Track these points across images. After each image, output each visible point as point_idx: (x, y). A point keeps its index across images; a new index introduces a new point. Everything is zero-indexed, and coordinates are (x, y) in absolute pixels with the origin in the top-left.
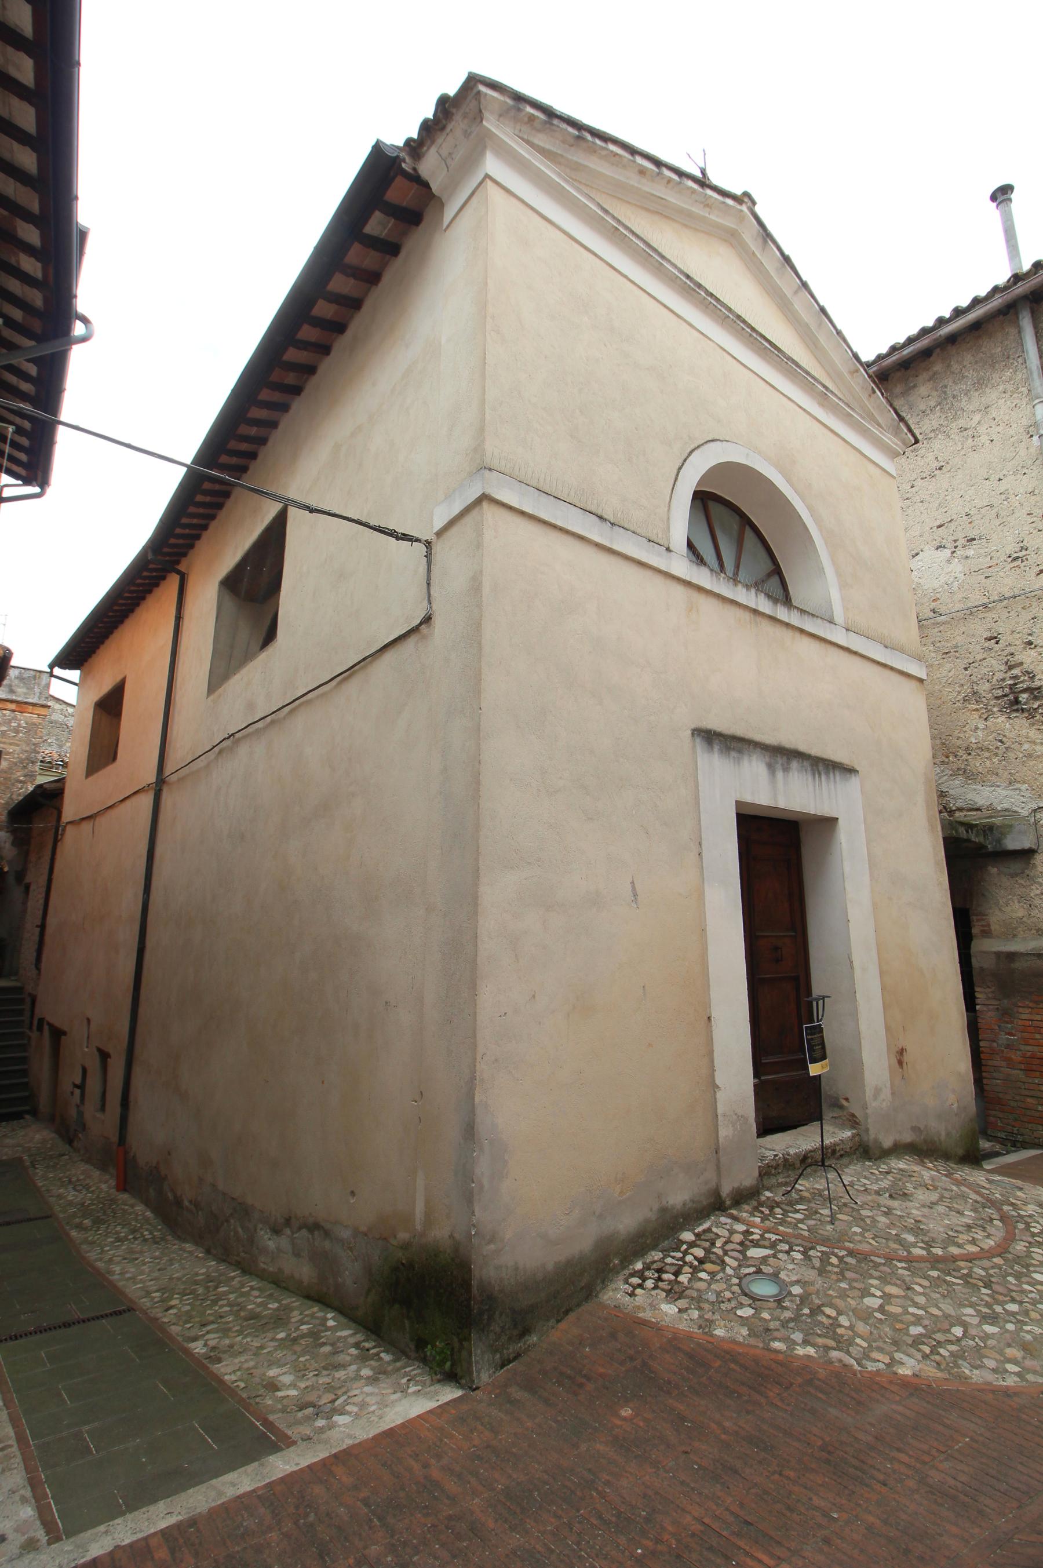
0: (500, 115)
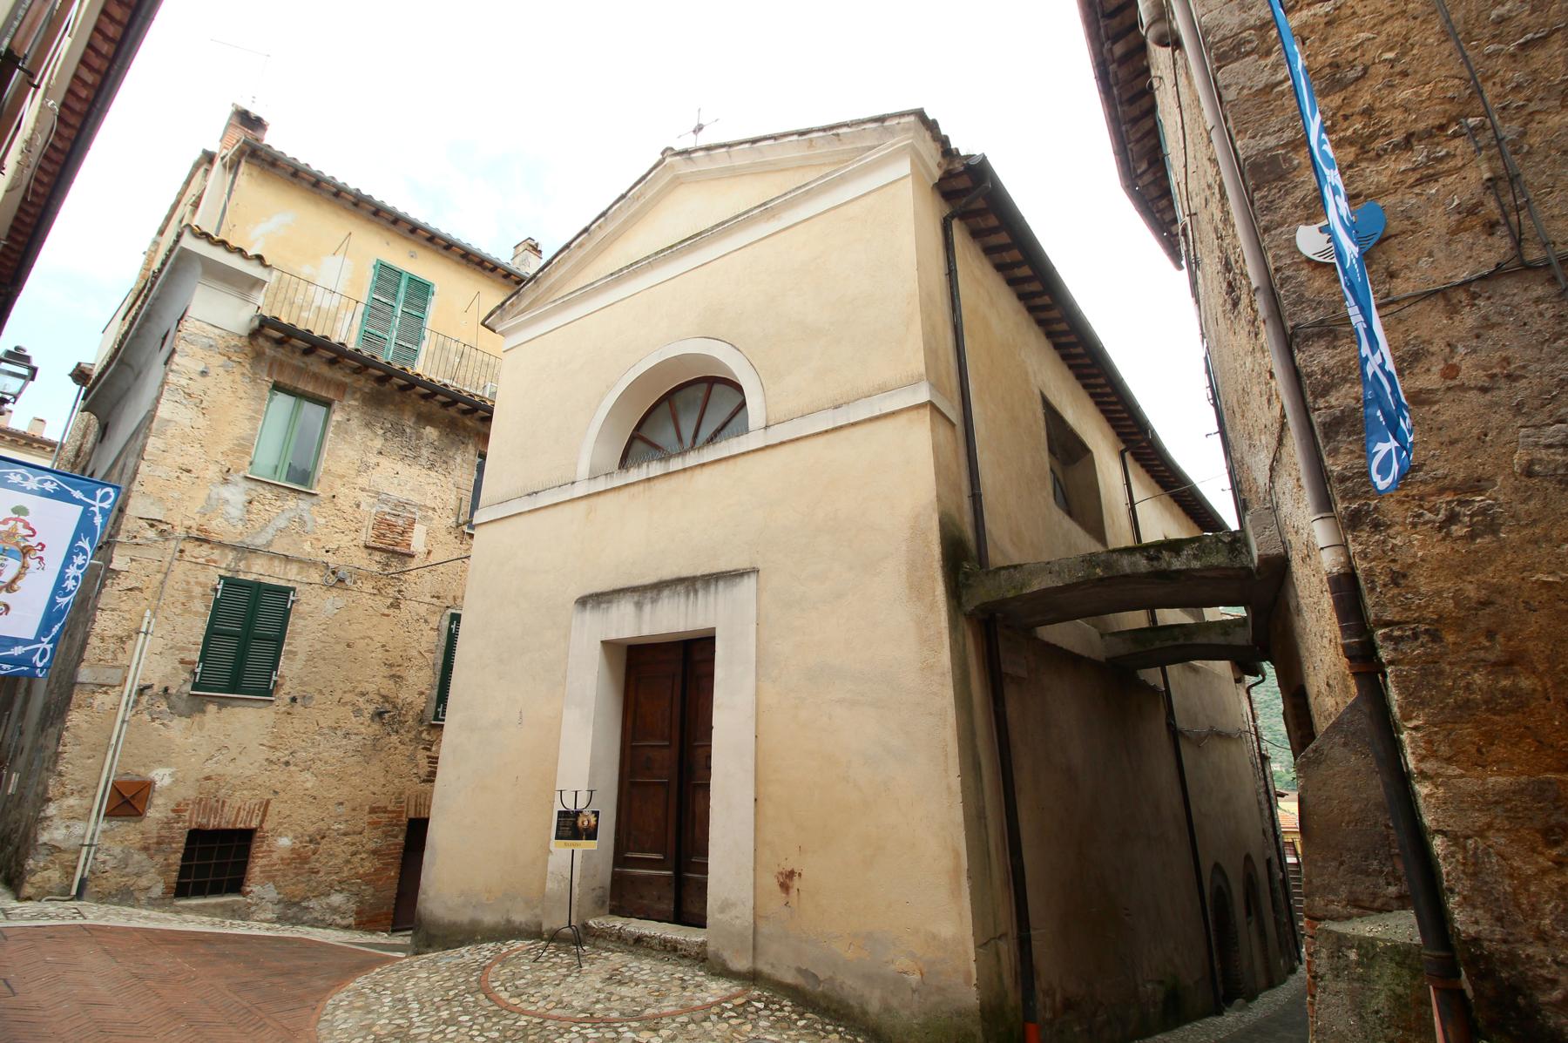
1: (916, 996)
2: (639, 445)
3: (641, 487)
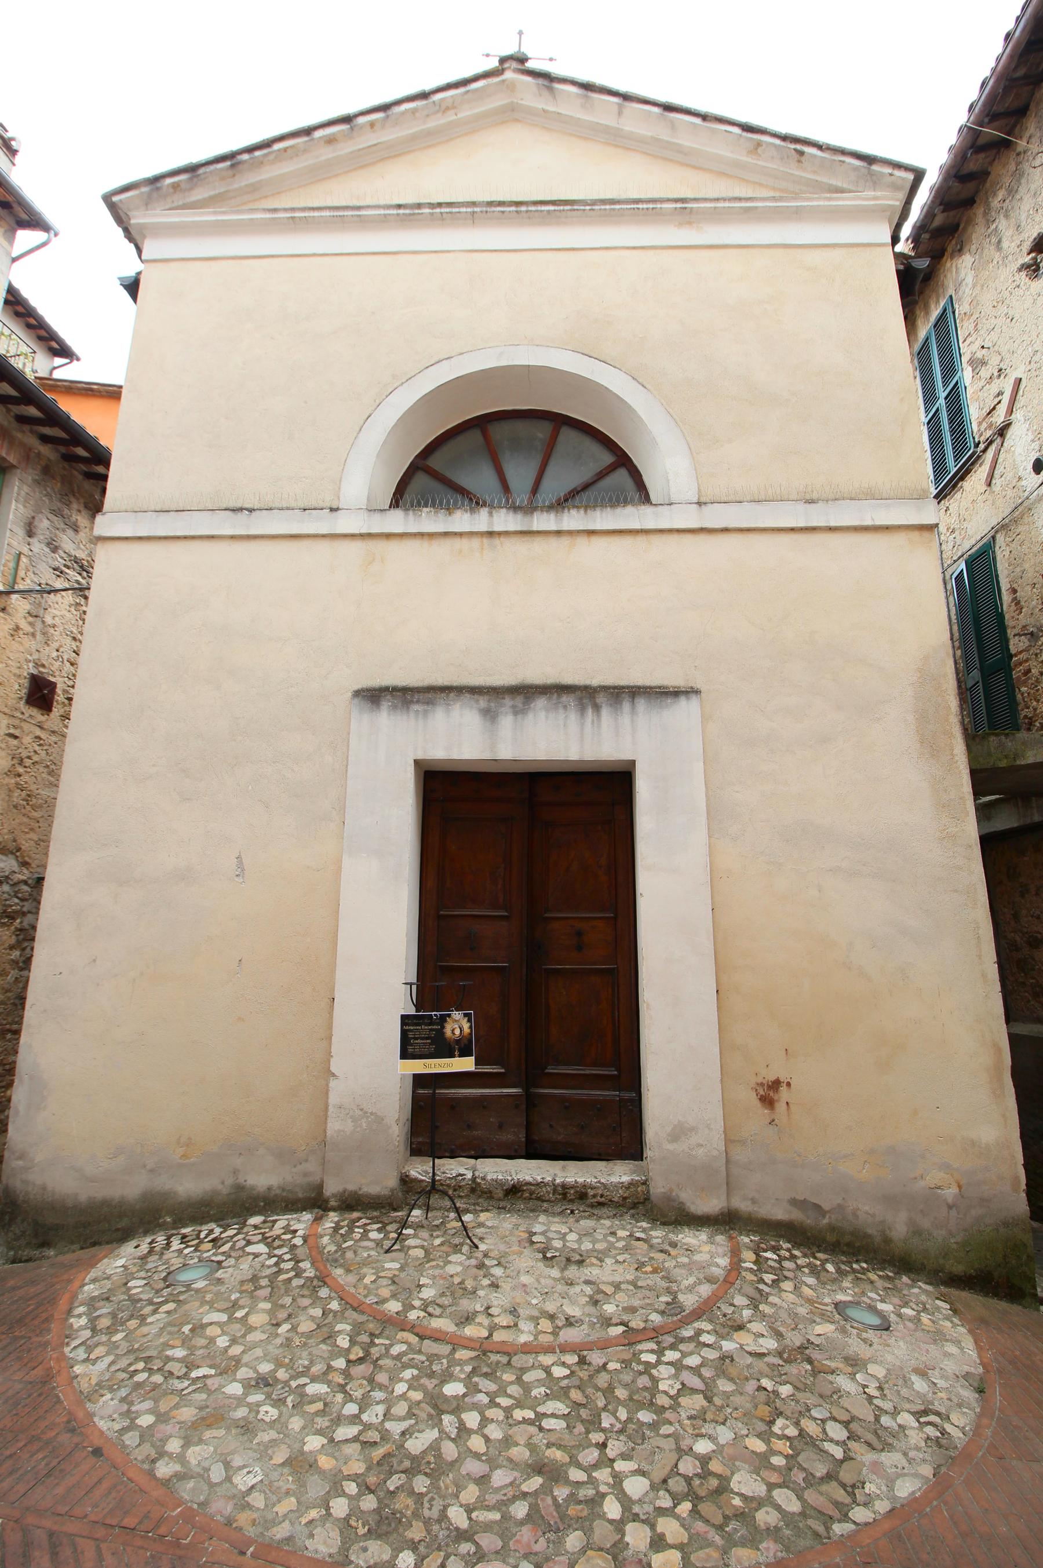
0: (147, 204)
1: (953, 1212)
2: (421, 480)
3: (476, 542)
